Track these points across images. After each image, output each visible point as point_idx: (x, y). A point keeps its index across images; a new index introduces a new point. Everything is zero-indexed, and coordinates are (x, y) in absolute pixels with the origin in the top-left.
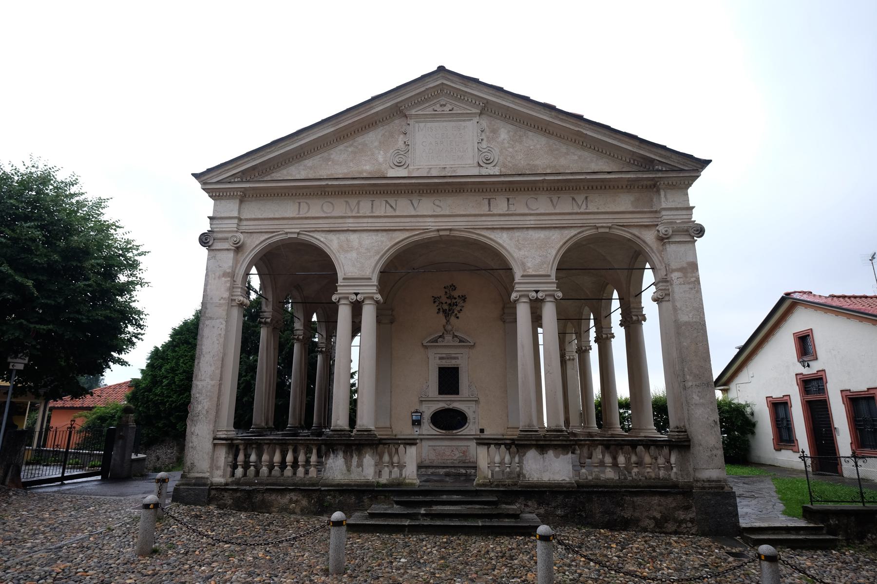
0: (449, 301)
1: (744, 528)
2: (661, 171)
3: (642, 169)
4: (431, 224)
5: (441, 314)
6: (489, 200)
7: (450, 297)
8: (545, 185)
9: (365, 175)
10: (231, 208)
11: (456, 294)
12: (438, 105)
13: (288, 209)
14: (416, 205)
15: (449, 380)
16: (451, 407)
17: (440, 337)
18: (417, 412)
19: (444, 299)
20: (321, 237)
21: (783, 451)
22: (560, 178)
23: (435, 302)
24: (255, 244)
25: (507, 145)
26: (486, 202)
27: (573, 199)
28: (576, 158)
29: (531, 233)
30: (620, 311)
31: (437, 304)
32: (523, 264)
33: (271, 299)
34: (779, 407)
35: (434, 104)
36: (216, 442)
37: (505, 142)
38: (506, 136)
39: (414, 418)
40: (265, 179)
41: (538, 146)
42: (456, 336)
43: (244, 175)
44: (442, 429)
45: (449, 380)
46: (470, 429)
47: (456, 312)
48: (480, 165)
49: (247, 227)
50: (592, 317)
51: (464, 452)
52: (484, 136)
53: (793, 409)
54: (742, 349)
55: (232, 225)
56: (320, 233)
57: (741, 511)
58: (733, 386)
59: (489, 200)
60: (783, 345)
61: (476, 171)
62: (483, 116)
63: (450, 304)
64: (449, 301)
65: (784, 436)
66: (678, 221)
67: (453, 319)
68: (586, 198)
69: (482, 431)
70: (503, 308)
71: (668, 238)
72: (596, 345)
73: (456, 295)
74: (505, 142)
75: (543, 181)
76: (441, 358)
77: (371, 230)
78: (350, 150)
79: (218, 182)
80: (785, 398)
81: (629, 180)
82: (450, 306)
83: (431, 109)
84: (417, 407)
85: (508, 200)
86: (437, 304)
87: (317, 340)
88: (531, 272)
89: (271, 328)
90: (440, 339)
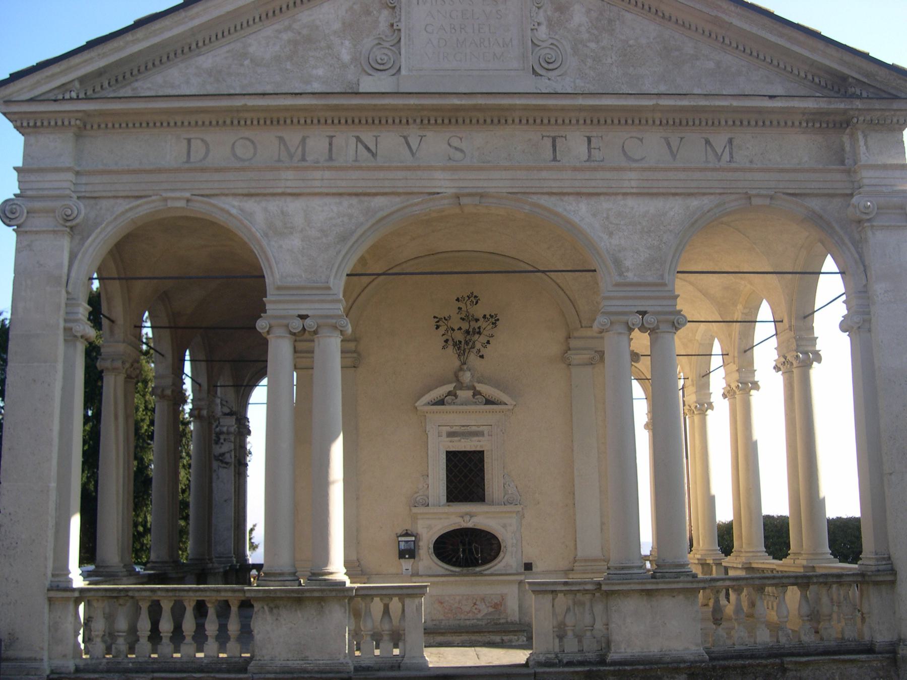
0: (465, 326)
2: (860, 97)
3: (832, 94)
4: (444, 183)
5: (450, 349)
6: (554, 140)
8: (658, 116)
9: (317, 87)
10: (59, 147)
11: (479, 311)
13: (168, 149)
15: (466, 476)
16: (470, 525)
18: (407, 534)
19: (455, 323)
20: (232, 205)
22: (685, 102)
23: (438, 327)
24: (111, 221)
25: (586, 36)
27: (707, 142)
29: (631, 202)
30: (774, 342)
31: (442, 329)
32: (617, 263)
36: (52, 594)
40: (122, 93)
42: (480, 393)
43: (94, 85)
44: (454, 565)
45: (466, 476)
46: (508, 560)
47: (478, 346)
48: (534, 72)
49: (89, 188)
50: (717, 348)
51: (496, 606)
52: (541, 18)
55: (64, 181)
56: (230, 199)
59: (554, 140)
61: (528, 84)
63: (468, 332)
64: (465, 326)
67: (473, 358)
68: (730, 141)
69: (528, 567)
70: (569, 337)
71: (869, 220)
73: (479, 315)
75: (654, 109)
76: (451, 434)
77: (327, 194)
78: (285, 36)
79: (32, 100)
82: (467, 334)
84: (408, 526)
85: (589, 140)
86: (442, 329)
88: (631, 277)
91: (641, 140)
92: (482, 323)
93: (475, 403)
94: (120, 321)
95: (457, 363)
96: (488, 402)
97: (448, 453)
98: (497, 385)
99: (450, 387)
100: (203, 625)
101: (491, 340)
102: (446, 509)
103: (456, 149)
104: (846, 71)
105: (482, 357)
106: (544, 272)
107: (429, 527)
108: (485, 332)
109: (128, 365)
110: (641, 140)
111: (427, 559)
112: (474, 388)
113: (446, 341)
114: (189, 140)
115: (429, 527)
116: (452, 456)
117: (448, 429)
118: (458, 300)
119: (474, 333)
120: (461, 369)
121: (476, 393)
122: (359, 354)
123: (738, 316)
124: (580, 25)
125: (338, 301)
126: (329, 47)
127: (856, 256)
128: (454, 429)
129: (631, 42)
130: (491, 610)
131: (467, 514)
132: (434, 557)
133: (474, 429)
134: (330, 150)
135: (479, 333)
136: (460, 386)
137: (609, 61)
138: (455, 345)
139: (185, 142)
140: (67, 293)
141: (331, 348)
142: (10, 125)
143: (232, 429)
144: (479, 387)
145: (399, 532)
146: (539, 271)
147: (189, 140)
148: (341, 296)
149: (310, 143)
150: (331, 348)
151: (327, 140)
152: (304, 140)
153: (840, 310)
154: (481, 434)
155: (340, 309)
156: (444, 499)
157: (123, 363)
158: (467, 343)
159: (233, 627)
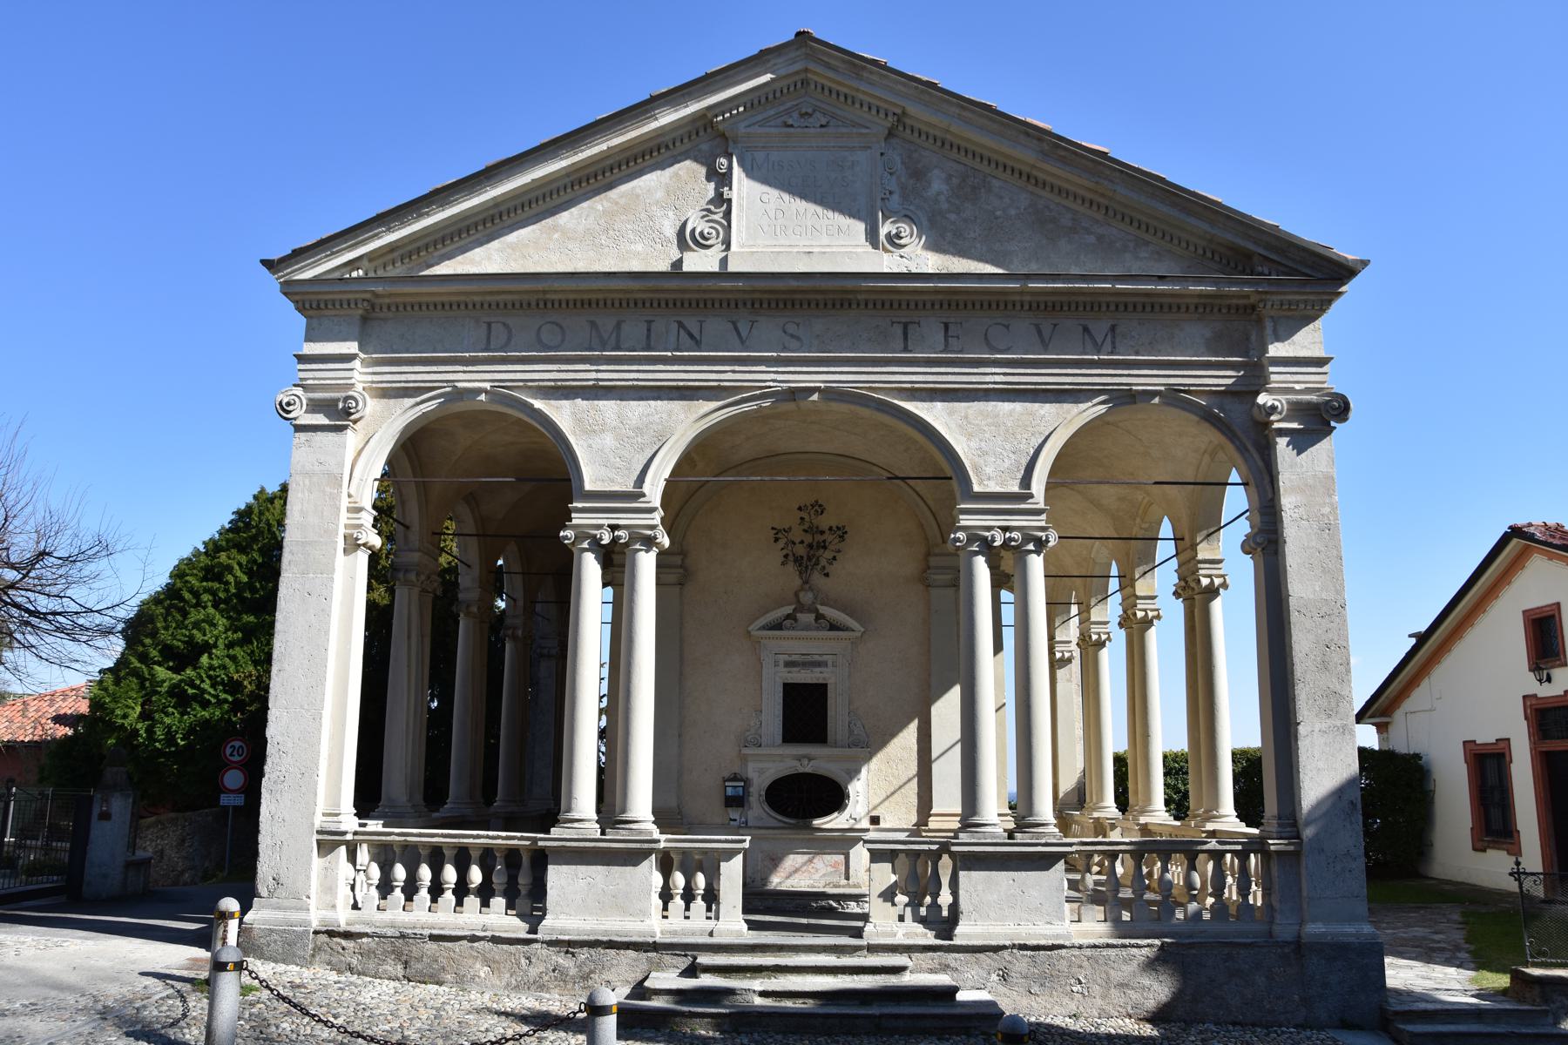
0: (808, 539)
1: (1397, 1013)
5: (791, 568)
6: (906, 326)
7: (812, 530)
11: (825, 522)
12: (795, 115)
14: (744, 334)
15: (805, 713)
16: (808, 769)
17: (788, 617)
18: (735, 778)
19: (797, 534)
21: (1490, 852)
23: (776, 540)
25: (945, 206)
26: (898, 330)
27: (1086, 330)
28: (1092, 239)
30: (1174, 563)
31: (781, 544)
33: (416, 527)
34: (1488, 764)
35: (788, 112)
37: (942, 198)
38: (944, 187)
39: (730, 791)
41: (1013, 212)
47: (823, 562)
50: (1114, 571)
53: (1513, 766)
54: (1422, 639)
57: (1388, 972)
58: (1399, 715)
59: (906, 326)
60: (1500, 635)
62: (894, 141)
63: (810, 546)
64: (808, 539)
65: (1494, 825)
66: (1297, 387)
68: (1113, 328)
70: (928, 554)
72: (1123, 632)
73: (824, 525)
74: (942, 198)
76: (788, 664)
80: (1502, 745)
81: (1200, 295)
83: (779, 121)
86: (781, 544)
87: (501, 604)
89: (416, 590)
90: (787, 623)
91: (1007, 327)
92: (828, 537)
93: (817, 629)
94: (416, 527)
95: (798, 582)
96: (833, 627)
97: (785, 685)
98: (844, 610)
99: (789, 610)
100: (516, 878)
101: (839, 556)
102: (780, 751)
103: (792, 336)
104: (1251, 246)
105: (827, 575)
106: (903, 479)
107: (761, 772)
108: (831, 547)
109: (423, 577)
110: (1007, 327)
111: (757, 809)
112: (817, 611)
113: (786, 556)
114: (489, 324)
115: (761, 772)
116: (791, 691)
117: (786, 658)
118: (800, 509)
119: (818, 548)
120: (802, 589)
121: (819, 617)
122: (686, 570)
123: (1136, 532)
124: (939, 194)
125: (652, 510)
126: (651, 218)
127: (1260, 464)
128: (794, 658)
129: (998, 213)
130: (830, 869)
131: (804, 756)
132: (767, 808)
133: (817, 658)
134: (648, 337)
135: (825, 548)
136: (801, 608)
137: (972, 235)
138: (796, 560)
139: (485, 326)
140: (350, 496)
141: (646, 565)
142: (292, 305)
143: (554, 652)
144: (823, 610)
145: (727, 774)
146: (897, 478)
147: (489, 324)
148: (657, 503)
149: (625, 328)
150: (646, 565)
151: (645, 327)
152: (618, 326)
153: (1243, 528)
154: (825, 664)
155: (657, 518)
156: (779, 739)
157: (418, 575)
158: (809, 559)
159: (524, 880)
